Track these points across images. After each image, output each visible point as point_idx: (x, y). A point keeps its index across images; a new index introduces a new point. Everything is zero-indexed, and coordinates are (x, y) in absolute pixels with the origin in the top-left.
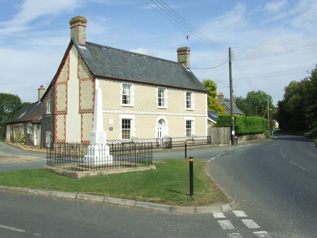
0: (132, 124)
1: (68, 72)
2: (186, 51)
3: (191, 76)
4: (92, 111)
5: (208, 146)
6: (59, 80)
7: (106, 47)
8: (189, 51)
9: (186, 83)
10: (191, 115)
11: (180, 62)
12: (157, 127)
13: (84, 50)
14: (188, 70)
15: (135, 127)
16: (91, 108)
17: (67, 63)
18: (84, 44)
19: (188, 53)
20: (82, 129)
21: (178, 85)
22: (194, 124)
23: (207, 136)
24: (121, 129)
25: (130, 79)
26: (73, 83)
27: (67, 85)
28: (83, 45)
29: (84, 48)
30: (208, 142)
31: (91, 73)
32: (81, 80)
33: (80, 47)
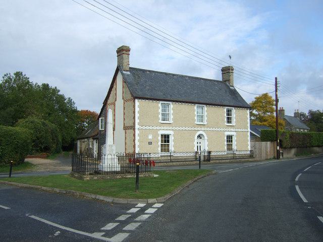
0: (171, 139)
1: (116, 94)
2: (229, 70)
3: (234, 93)
4: (133, 128)
5: (250, 160)
6: (109, 101)
7: (149, 71)
8: (233, 70)
9: (228, 99)
10: (232, 130)
11: (225, 80)
12: (196, 141)
13: (128, 75)
14: (231, 88)
15: (139, 141)
16: (132, 125)
17: (115, 86)
18: (128, 69)
19: (231, 71)
20: (126, 143)
21: (218, 102)
22: (173, 138)
23: (250, 150)
24: (226, 143)
25: (169, 98)
26: (120, 103)
27: (115, 106)
28: (127, 71)
29: (129, 73)
30: (251, 156)
31: (132, 96)
32: (125, 100)
33: (124, 72)
